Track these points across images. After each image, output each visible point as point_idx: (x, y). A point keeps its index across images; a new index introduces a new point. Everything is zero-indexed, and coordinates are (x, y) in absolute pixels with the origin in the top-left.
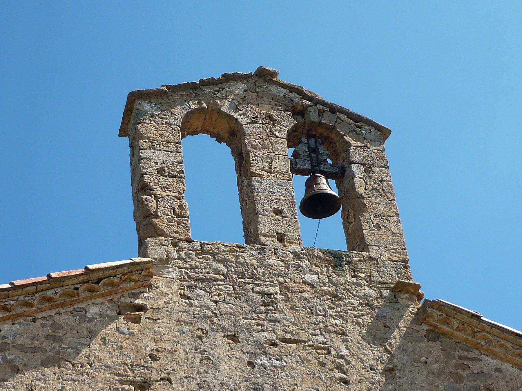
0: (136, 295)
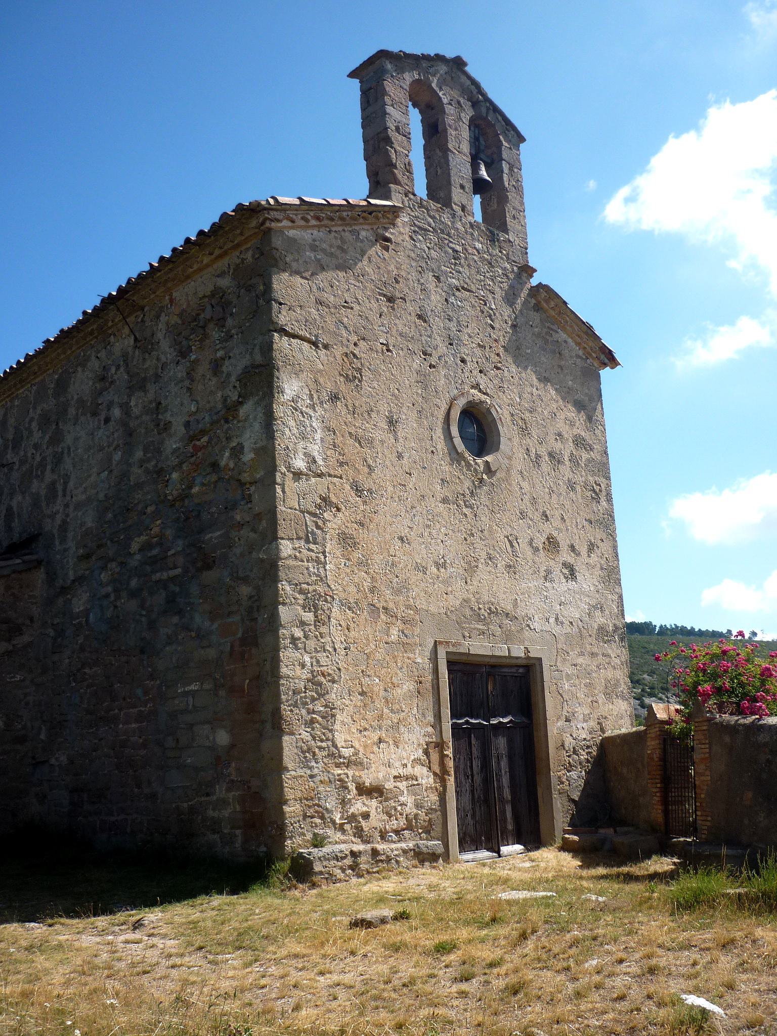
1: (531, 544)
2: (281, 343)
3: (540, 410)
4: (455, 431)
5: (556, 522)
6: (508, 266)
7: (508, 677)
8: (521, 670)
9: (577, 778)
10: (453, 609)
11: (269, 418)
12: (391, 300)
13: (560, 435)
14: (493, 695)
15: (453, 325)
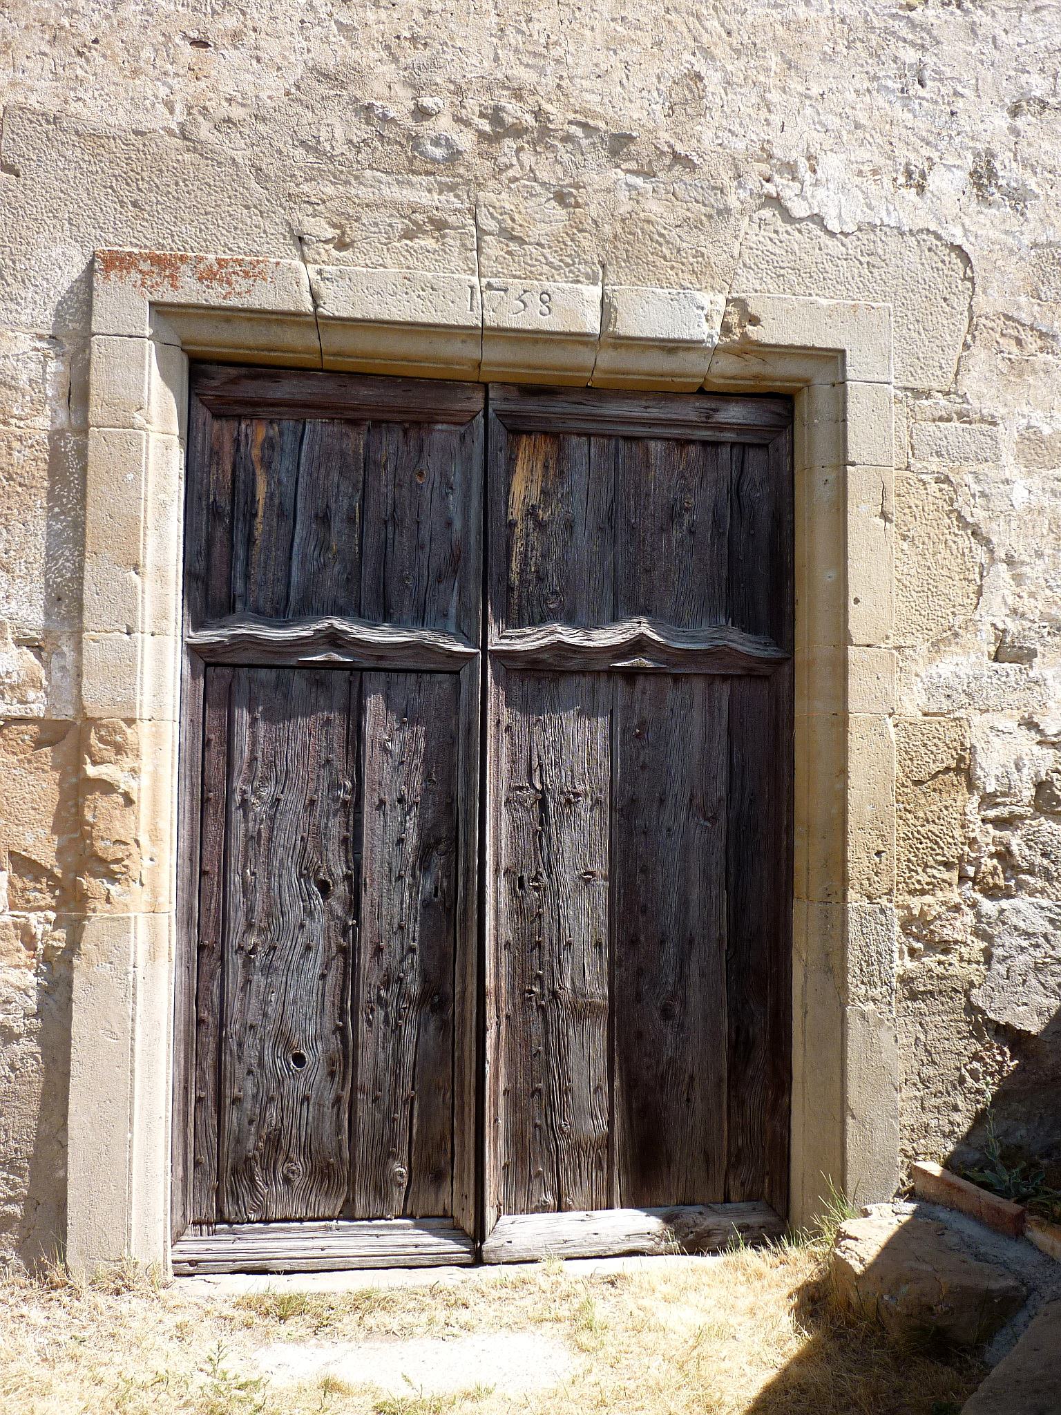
7: (656, 448)
8: (734, 413)
9: (1044, 926)
10: (237, 113)
14: (541, 526)
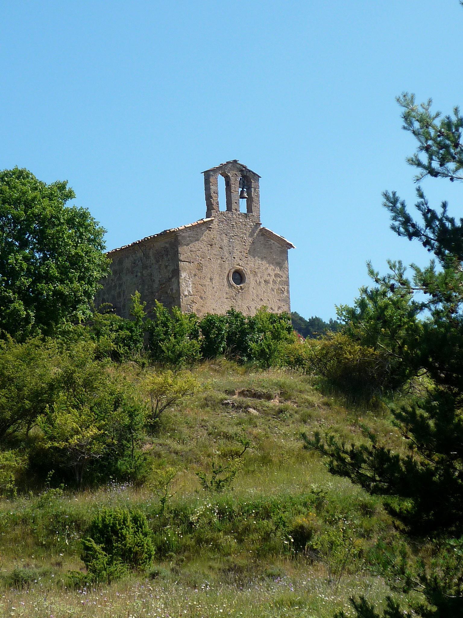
0: (210, 225)
1: (256, 308)
2: (181, 264)
3: (261, 268)
4: (231, 279)
5: (265, 301)
6: (252, 224)
11: (179, 283)
12: (211, 245)
13: (269, 274)
15: (231, 248)
